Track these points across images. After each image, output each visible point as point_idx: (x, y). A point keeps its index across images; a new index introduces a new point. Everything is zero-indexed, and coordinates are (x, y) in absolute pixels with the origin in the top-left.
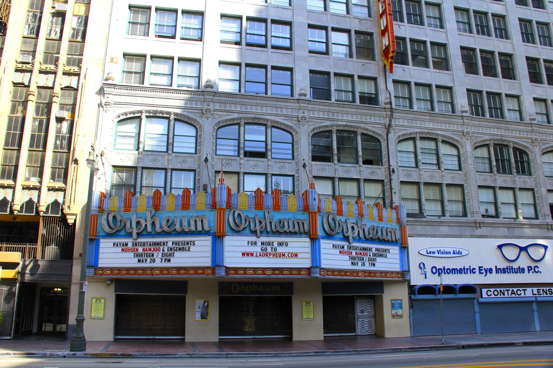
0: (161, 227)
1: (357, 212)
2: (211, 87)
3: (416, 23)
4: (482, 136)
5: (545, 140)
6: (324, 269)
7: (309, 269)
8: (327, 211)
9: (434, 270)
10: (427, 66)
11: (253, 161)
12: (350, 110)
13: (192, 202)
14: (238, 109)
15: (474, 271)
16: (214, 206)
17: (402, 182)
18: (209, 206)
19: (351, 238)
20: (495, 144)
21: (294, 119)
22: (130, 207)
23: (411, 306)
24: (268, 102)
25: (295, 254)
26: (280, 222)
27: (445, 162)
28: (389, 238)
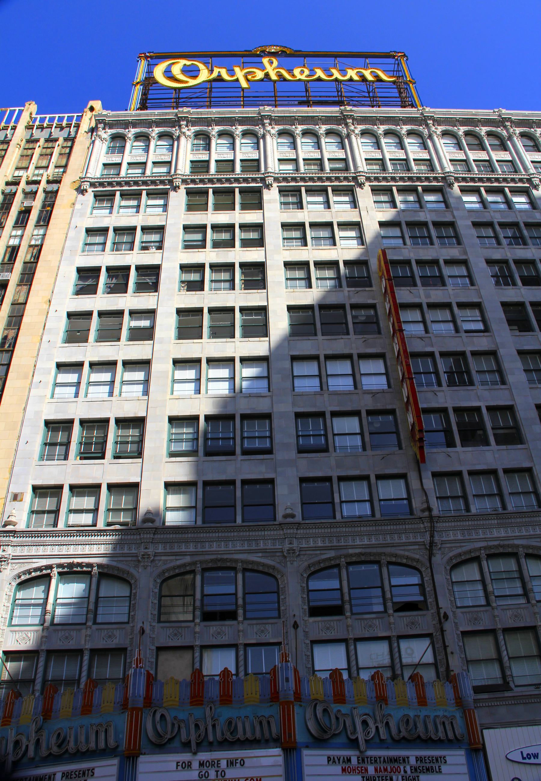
2: (153, 521)
3: (462, 383)
8: (312, 697)
10: (488, 444)
11: (214, 627)
12: (365, 529)
13: (95, 701)
14: (192, 548)
16: (124, 705)
17: (465, 634)
19: (361, 742)
21: (278, 554)
24: (236, 534)
26: (230, 723)
27: (536, 589)
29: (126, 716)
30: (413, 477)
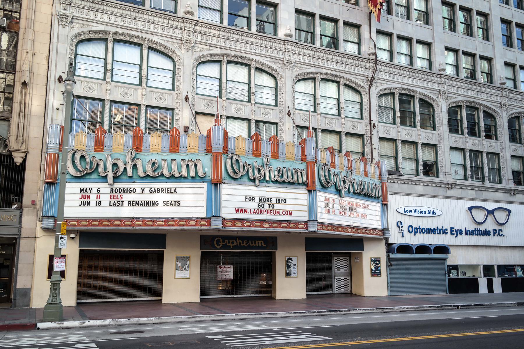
0: (145, 171)
1: (347, 166)
4: (457, 96)
5: (512, 105)
6: (319, 223)
7: (306, 222)
9: (411, 229)
13: (182, 143)
15: (446, 232)
16: (209, 150)
18: (204, 149)
20: (468, 106)
22: (103, 146)
23: (389, 266)
25: (294, 205)
28: (373, 194)
29: (210, 156)
30: (365, 30)
